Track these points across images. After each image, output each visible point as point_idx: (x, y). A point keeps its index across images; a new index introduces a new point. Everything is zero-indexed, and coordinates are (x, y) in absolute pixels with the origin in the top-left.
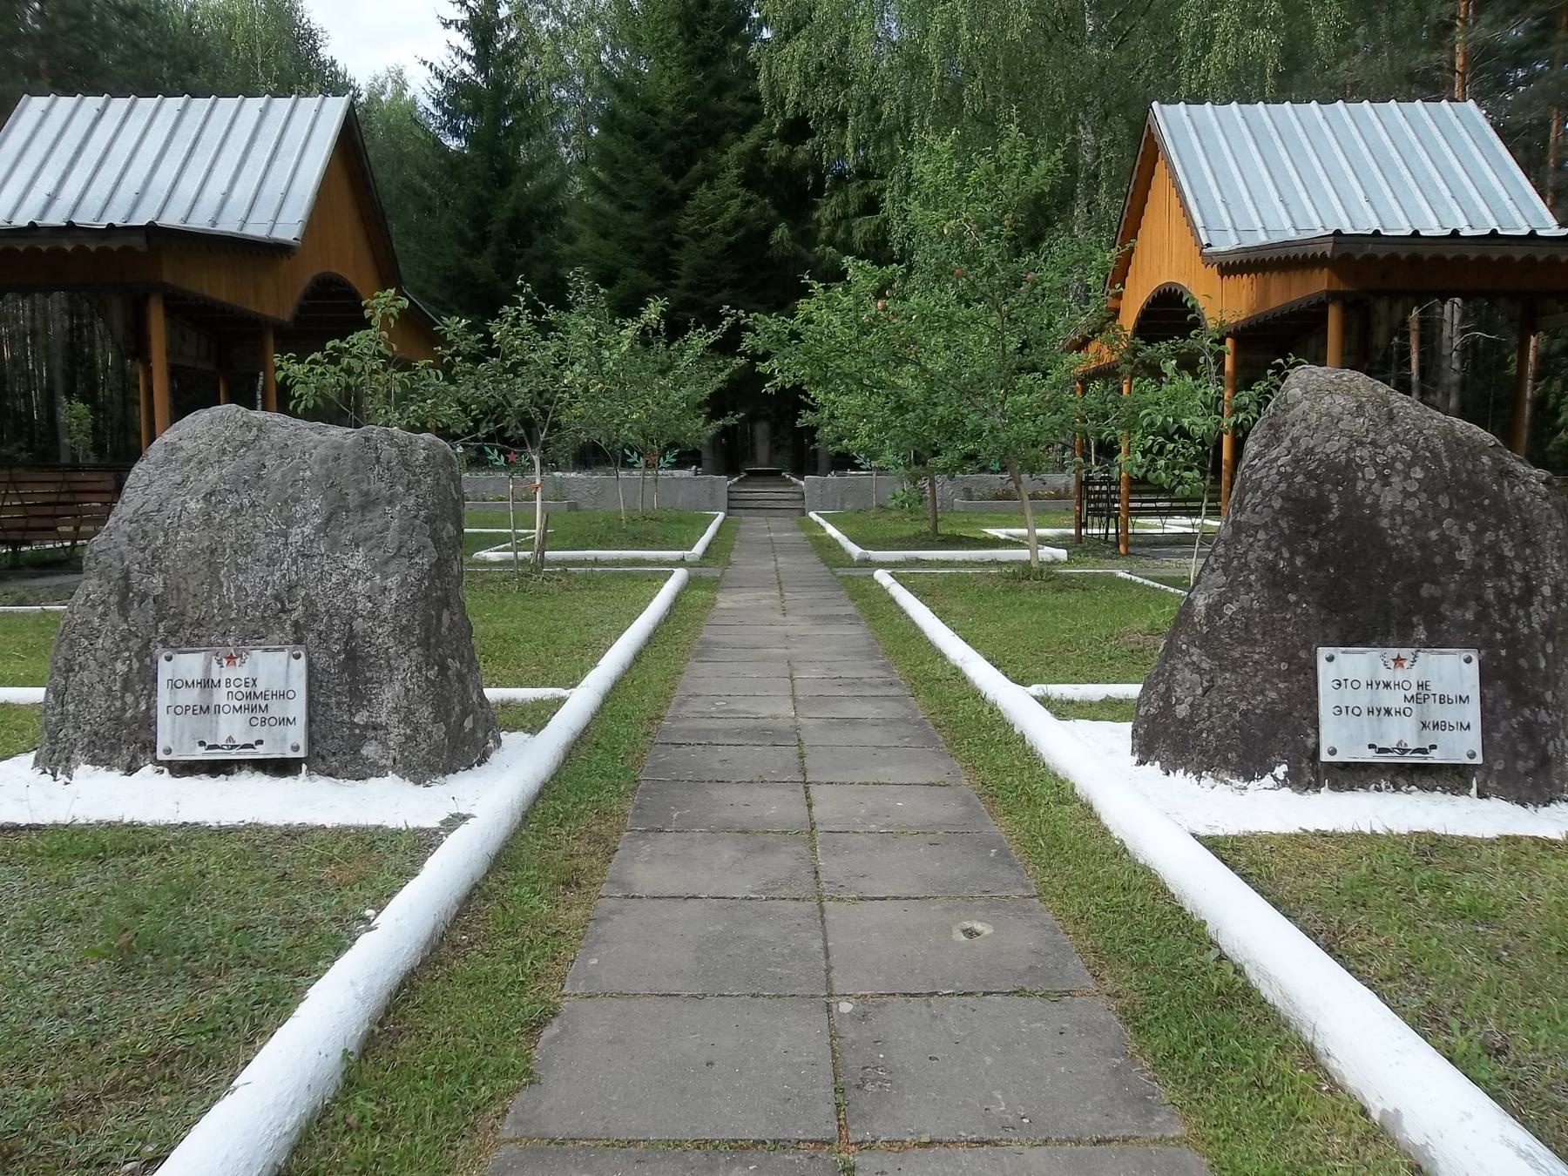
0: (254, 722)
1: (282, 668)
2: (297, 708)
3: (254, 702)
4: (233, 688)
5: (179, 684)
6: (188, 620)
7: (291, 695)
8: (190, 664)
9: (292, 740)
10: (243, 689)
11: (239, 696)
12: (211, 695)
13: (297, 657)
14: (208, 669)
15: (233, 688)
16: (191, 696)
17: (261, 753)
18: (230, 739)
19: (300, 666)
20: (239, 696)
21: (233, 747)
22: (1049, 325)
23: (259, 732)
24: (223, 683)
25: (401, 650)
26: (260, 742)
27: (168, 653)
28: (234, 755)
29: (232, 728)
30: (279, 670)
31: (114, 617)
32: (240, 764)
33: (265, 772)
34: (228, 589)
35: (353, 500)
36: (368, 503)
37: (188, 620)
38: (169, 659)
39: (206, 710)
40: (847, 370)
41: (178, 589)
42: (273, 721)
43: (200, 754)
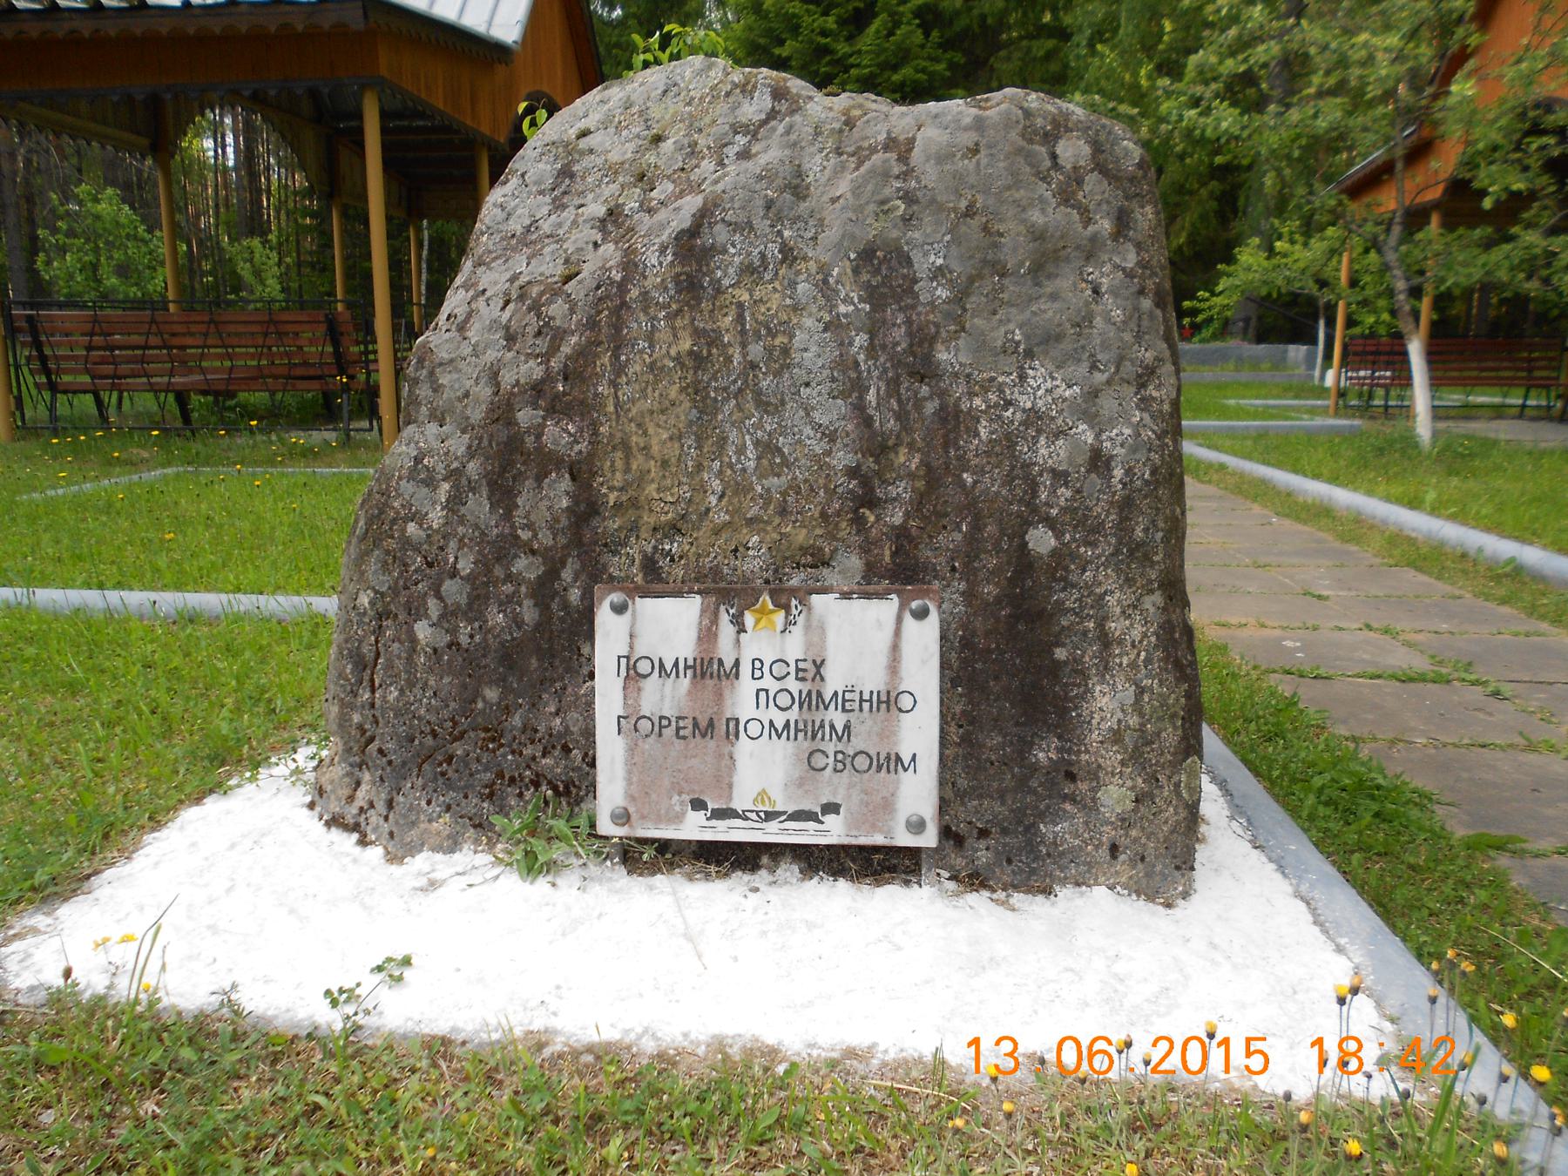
0: (819, 761)
1: (884, 637)
2: (920, 733)
3: (811, 706)
4: (768, 682)
5: (644, 667)
6: (648, 519)
7: (906, 701)
8: (670, 624)
9: (914, 804)
10: (793, 685)
11: (784, 700)
12: (719, 696)
13: (921, 614)
14: (707, 635)
15: (768, 682)
16: (664, 697)
17: (833, 831)
18: (762, 795)
19: (923, 641)
20: (784, 700)
21: (770, 816)
22: (1096, 291)
23: (833, 787)
24: (745, 669)
25: (1128, 597)
26: (831, 808)
27: (616, 597)
28: (772, 833)
29: (762, 773)
30: (881, 646)
31: (479, 506)
32: (776, 852)
33: (838, 872)
34: (741, 451)
35: (1015, 251)
36: (1047, 258)
37: (648, 519)
38: (619, 609)
39: (705, 729)
40: (685, 411)
41: (625, 446)
42: (862, 762)
43: (694, 828)
